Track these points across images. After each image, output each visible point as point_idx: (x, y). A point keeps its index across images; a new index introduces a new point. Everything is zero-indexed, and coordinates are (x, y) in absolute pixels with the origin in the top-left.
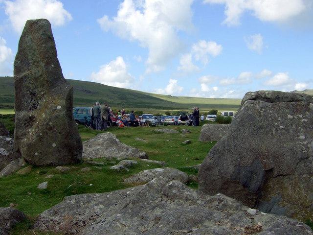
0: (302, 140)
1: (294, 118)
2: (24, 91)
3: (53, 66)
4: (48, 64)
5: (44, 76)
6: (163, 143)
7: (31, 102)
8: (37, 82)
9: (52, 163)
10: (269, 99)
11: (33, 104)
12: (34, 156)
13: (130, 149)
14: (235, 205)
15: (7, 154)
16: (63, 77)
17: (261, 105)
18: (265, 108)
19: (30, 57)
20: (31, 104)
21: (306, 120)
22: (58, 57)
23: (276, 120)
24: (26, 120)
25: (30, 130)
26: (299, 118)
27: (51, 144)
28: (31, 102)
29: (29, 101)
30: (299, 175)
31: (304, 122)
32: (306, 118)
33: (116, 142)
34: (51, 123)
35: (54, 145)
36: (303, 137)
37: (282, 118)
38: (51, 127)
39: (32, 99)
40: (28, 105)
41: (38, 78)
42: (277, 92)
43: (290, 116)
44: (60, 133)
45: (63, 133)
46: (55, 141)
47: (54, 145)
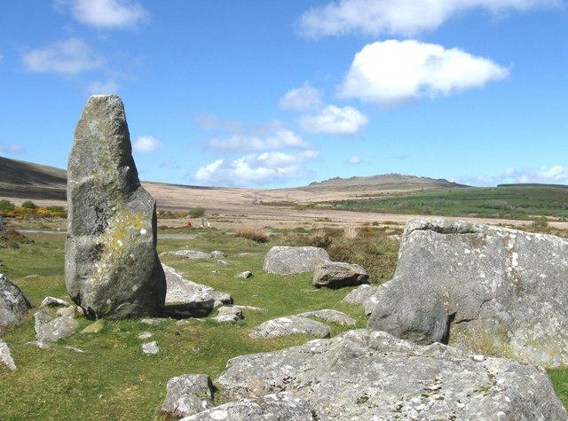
4: (122, 165)
13: (204, 290)
20: (96, 226)
36: (483, 276)
43: (467, 251)
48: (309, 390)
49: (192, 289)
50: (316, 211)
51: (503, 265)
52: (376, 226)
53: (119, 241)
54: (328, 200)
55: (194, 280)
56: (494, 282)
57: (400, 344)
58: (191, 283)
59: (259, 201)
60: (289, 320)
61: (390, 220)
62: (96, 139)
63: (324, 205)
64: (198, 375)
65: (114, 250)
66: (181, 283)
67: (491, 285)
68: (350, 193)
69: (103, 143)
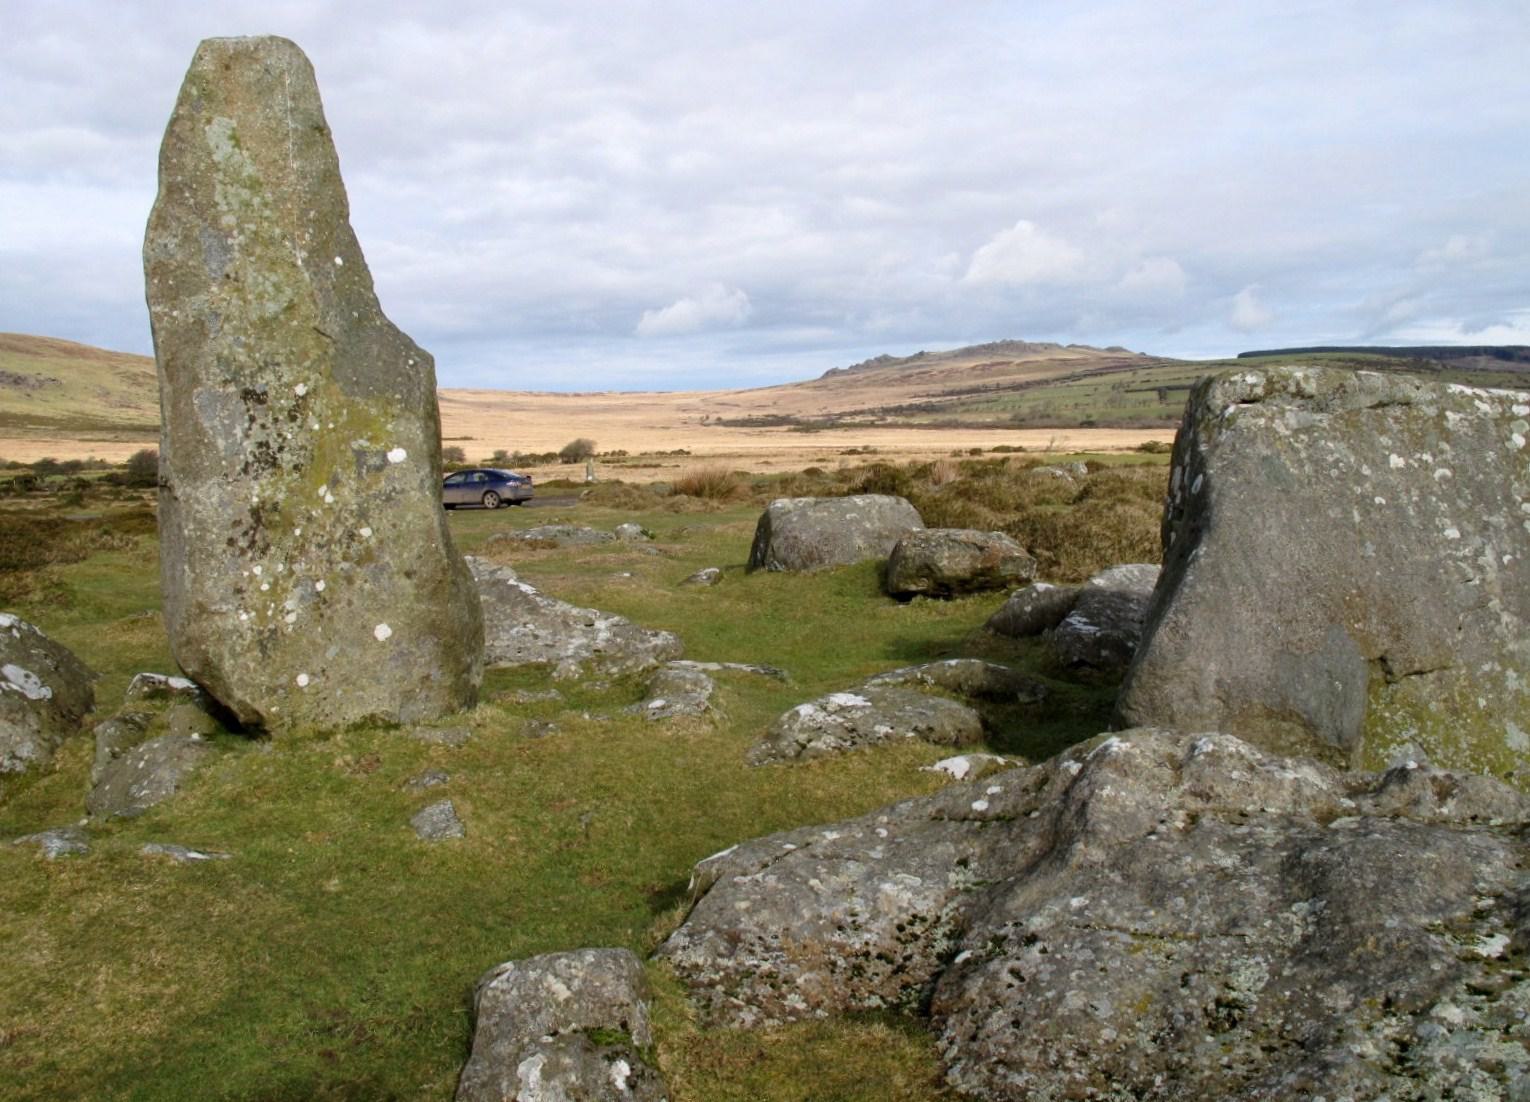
0: (1456, 544)
1: (1408, 466)
2: (212, 378)
3: (339, 261)
4: (318, 254)
5: (305, 309)
6: (419, 563)
7: (247, 436)
8: (271, 338)
9: (373, 716)
10: (1311, 397)
11: (260, 445)
12: (292, 688)
13: (600, 624)
14: (337, 804)
15: (46, 693)
16: (380, 314)
17: (1292, 421)
18: (1308, 429)
19: (228, 220)
20: (249, 446)
21: (1448, 473)
22: (353, 221)
23: (1360, 479)
24: (237, 523)
25: (257, 570)
26: (1424, 465)
27: (367, 629)
28: (247, 436)
29: (238, 432)
30: (1468, 665)
31: (1443, 478)
32: (1445, 464)
33: (525, 595)
34: (366, 532)
35: (383, 632)
36: (1453, 533)
37: (1373, 465)
38: (368, 549)
39: (252, 419)
40: (235, 451)
41: (275, 318)
42: (365, 266)
43: (1396, 461)
44: (408, 575)
45: (425, 572)
46: (382, 611)
47: (383, 632)
48: (1007, 978)
49: (566, 624)
50: (839, 433)
51: (1508, 498)
52: (976, 458)
53: (322, 490)
54: (865, 407)
55: (569, 601)
56: (1488, 551)
57: (1290, 775)
58: (561, 607)
59: (713, 417)
60: (859, 701)
61: (1006, 444)
62: (777, 891)
63: (858, 419)
64: (590, 957)
65: (310, 519)
66: (533, 609)
67: (1481, 561)
68: (914, 389)
69: (254, 185)
